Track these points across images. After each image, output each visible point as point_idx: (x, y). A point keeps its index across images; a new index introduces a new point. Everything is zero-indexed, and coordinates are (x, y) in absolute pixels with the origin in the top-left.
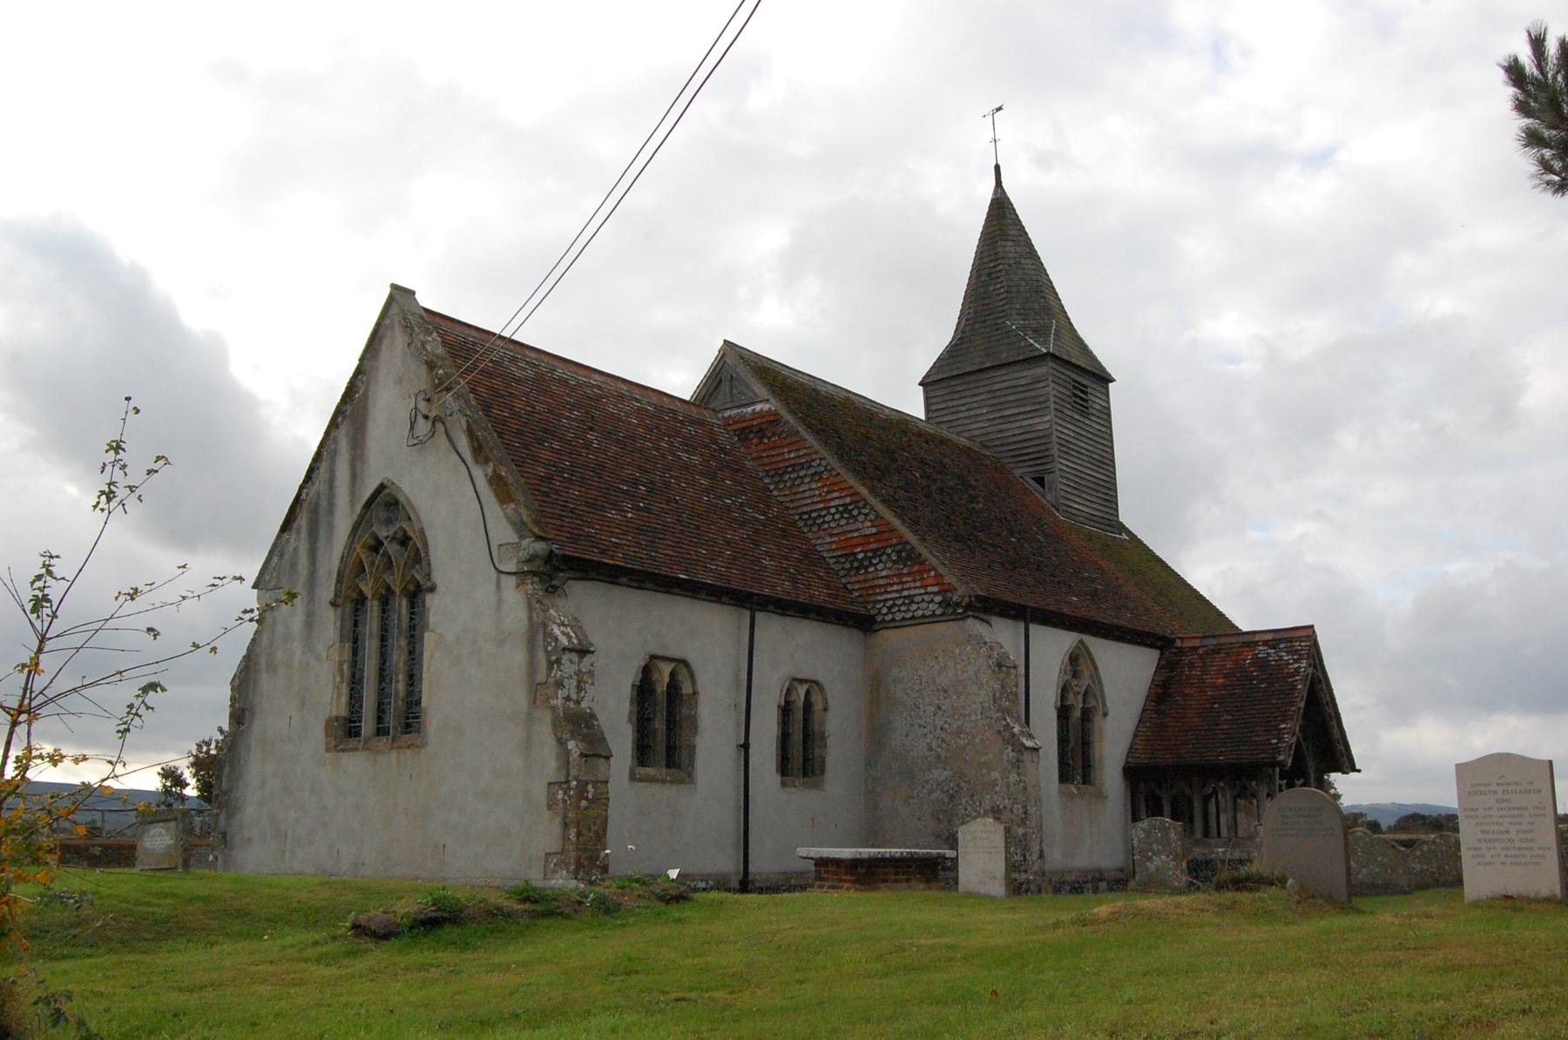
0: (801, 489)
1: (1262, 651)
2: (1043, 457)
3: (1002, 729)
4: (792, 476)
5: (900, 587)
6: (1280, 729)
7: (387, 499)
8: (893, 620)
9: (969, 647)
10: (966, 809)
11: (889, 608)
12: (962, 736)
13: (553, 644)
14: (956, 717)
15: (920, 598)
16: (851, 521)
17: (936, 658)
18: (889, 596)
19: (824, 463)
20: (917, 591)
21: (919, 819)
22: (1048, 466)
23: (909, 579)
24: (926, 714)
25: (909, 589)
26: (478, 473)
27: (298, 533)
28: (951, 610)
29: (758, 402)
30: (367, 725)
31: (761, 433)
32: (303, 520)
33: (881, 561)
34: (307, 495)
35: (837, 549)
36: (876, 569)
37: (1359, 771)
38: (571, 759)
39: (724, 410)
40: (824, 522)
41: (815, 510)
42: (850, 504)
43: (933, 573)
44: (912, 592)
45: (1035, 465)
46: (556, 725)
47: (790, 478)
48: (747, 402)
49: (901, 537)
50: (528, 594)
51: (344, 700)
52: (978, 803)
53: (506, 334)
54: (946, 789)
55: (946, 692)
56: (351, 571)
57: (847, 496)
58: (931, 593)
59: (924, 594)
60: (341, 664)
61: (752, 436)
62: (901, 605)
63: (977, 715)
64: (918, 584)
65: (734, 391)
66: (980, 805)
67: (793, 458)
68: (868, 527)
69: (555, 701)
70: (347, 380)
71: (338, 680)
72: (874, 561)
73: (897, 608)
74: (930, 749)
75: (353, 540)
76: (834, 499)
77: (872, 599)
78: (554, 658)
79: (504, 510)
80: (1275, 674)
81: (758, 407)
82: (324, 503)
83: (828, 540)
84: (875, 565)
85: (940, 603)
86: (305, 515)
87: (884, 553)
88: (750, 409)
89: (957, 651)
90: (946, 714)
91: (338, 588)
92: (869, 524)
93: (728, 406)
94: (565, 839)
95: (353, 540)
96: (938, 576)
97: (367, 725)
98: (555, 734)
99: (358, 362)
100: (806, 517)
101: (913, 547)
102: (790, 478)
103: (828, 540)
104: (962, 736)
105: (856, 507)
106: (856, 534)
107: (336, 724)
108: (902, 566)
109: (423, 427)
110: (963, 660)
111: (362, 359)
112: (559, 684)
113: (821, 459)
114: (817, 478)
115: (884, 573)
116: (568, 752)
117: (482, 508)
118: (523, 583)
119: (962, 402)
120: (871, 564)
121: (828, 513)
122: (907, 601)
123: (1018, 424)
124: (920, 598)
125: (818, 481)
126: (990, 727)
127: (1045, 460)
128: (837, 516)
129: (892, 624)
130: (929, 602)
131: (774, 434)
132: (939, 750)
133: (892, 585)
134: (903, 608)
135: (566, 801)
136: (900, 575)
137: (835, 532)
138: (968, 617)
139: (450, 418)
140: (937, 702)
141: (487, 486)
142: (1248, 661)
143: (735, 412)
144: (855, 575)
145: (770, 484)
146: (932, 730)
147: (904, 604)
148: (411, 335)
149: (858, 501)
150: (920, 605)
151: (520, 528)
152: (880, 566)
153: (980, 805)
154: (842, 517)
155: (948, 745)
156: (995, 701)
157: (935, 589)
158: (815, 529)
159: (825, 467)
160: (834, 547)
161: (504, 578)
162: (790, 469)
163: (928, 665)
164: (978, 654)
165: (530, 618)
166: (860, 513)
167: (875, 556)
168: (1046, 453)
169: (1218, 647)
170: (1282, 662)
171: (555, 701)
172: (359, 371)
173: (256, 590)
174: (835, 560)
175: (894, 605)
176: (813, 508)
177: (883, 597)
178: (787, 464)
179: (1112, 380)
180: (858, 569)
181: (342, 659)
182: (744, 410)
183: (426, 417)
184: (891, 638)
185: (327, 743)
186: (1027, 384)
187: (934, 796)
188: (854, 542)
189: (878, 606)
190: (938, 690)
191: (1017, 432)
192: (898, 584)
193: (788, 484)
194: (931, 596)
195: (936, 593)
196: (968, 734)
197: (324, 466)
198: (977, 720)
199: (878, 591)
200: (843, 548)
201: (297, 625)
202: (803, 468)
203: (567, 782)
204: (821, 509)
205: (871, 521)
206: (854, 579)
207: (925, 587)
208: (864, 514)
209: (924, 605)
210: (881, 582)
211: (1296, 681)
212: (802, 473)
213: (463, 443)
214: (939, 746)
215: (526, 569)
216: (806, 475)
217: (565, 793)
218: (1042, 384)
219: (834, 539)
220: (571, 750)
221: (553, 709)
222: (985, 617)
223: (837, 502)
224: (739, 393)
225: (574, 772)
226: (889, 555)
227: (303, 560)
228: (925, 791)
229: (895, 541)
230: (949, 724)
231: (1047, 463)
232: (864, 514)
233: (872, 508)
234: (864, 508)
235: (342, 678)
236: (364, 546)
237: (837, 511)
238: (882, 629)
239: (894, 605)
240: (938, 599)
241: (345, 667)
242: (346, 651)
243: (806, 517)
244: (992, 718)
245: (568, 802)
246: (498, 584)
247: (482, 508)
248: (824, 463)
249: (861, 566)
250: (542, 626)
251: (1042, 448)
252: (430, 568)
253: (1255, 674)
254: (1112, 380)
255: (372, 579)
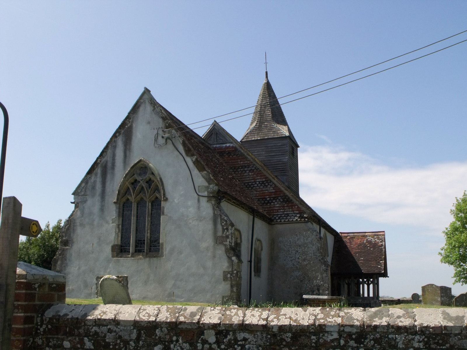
0: (245, 175)
1: (370, 238)
2: (284, 170)
3: (321, 259)
4: (241, 170)
5: (283, 211)
6: (380, 263)
7: (142, 166)
8: (292, 220)
9: (309, 232)
10: (307, 285)
11: (279, 218)
12: (306, 261)
13: (225, 223)
14: (304, 255)
15: (291, 215)
16: (265, 187)
17: (297, 235)
18: (279, 213)
19: (254, 166)
20: (290, 212)
21: (289, 288)
22: (286, 174)
23: (288, 208)
24: (292, 253)
25: (287, 211)
26: (189, 160)
27: (96, 175)
28: (303, 220)
29: (228, 143)
30: (132, 249)
31: (229, 153)
32: (99, 170)
33: (276, 201)
34: (100, 161)
35: (259, 196)
36: (274, 204)
37: (388, 277)
38: (234, 263)
39: (213, 144)
40: (254, 186)
41: (251, 182)
42: (264, 181)
43: (296, 207)
44: (288, 212)
45: (282, 173)
46: (227, 251)
47: (240, 170)
48: (223, 143)
49: (284, 194)
50: (212, 205)
51: (120, 238)
52: (311, 283)
53: (280, 101)
54: (299, 278)
55: (300, 246)
56: (123, 193)
57: (263, 178)
58: (296, 213)
59: (293, 213)
60: (118, 225)
61: (225, 154)
62: (283, 217)
63: (311, 254)
64: (291, 210)
65: (218, 138)
66: (312, 283)
67: (242, 164)
68: (272, 190)
69: (226, 243)
70: (122, 120)
71: (117, 231)
72: (273, 201)
73: (282, 218)
74: (294, 265)
75: (125, 179)
76: (258, 179)
77: (272, 214)
78: (225, 228)
79: (201, 174)
80: (375, 245)
81: (228, 145)
82: (109, 165)
83: (255, 193)
84: (274, 202)
85: (299, 217)
86: (99, 169)
87: (278, 199)
88: (224, 145)
89: (305, 233)
90: (300, 254)
91: (118, 197)
92: (272, 188)
93: (215, 143)
94: (232, 291)
95: (125, 179)
96: (298, 207)
97: (132, 249)
98: (227, 255)
99: (127, 114)
100: (247, 184)
101: (289, 197)
102: (240, 170)
103: (255, 193)
104: (306, 261)
105: (267, 182)
106: (267, 192)
107: (117, 247)
108: (284, 203)
109: (161, 141)
110: (306, 236)
111: (129, 113)
112: (227, 237)
113: (253, 165)
114: (252, 171)
115: (277, 205)
116: (232, 261)
117: (190, 172)
118: (210, 200)
119: (255, 149)
120: (272, 202)
121: (256, 184)
122: (286, 215)
123: (276, 159)
124: (291, 215)
125: (252, 172)
126: (317, 258)
127: (284, 171)
128: (259, 185)
129: (280, 223)
130: (295, 216)
131: (234, 155)
132: (297, 266)
133: (280, 210)
134: (284, 218)
135: (232, 278)
136: (284, 207)
137: (258, 190)
138: (309, 222)
139: (174, 139)
140: (297, 249)
141: (193, 165)
142: (365, 241)
143: (218, 146)
144: (265, 205)
145: (232, 172)
146: (295, 259)
147: (285, 216)
148: (154, 107)
149: (268, 181)
150: (291, 217)
151: (209, 181)
152: (276, 203)
153: (312, 283)
154: (261, 185)
155: (300, 264)
156: (318, 250)
157: (298, 212)
158: (250, 189)
159: (255, 168)
160: (258, 195)
161: (201, 198)
162: (241, 167)
163: (293, 237)
164: (313, 234)
165: (214, 213)
166: (268, 185)
167: (274, 199)
168: (285, 169)
169: (354, 236)
170: (376, 242)
171: (226, 243)
172: (128, 118)
173: (73, 196)
174: (258, 200)
175: (281, 216)
176: (250, 181)
177: (277, 214)
178: (239, 165)
179: (299, 147)
180: (267, 204)
181: (119, 223)
182: (222, 145)
183: (163, 137)
184: (280, 227)
185: (112, 254)
186: (279, 146)
187: (295, 281)
188: (266, 194)
189: (274, 216)
190: (297, 245)
191: (275, 161)
192: (283, 209)
193: (240, 172)
194: (296, 214)
195: (297, 214)
196: (308, 260)
197: (109, 151)
198: (311, 256)
199: (275, 211)
200: (261, 196)
201: (96, 209)
202: (246, 167)
203: (233, 271)
204: (253, 182)
205: (273, 187)
206: (265, 207)
207: (293, 211)
208: (270, 185)
209: (293, 217)
210: (276, 208)
211: (382, 248)
212: (246, 169)
213: (181, 148)
214: (297, 264)
215: (211, 195)
216: (247, 170)
217: (231, 275)
218: (285, 146)
219: (258, 193)
220: (234, 260)
221: (225, 245)
222: (312, 222)
223: (259, 180)
224: (220, 139)
225: (235, 267)
226: (279, 200)
227: (99, 186)
228: (292, 279)
229: (282, 195)
230: (301, 257)
231: (286, 173)
232: (270, 185)
233: (273, 183)
234: (270, 183)
235: (119, 230)
236: (129, 183)
237: (259, 183)
238: (277, 224)
239: (281, 216)
240: (298, 215)
241: (120, 226)
242: (120, 221)
243: (247, 184)
244: (317, 255)
245: (233, 278)
246: (199, 201)
247: (190, 172)
248: (254, 166)
249: (268, 202)
250: (219, 216)
251: (284, 167)
252: (165, 192)
253: (368, 245)
254: (299, 147)
255: (134, 195)
